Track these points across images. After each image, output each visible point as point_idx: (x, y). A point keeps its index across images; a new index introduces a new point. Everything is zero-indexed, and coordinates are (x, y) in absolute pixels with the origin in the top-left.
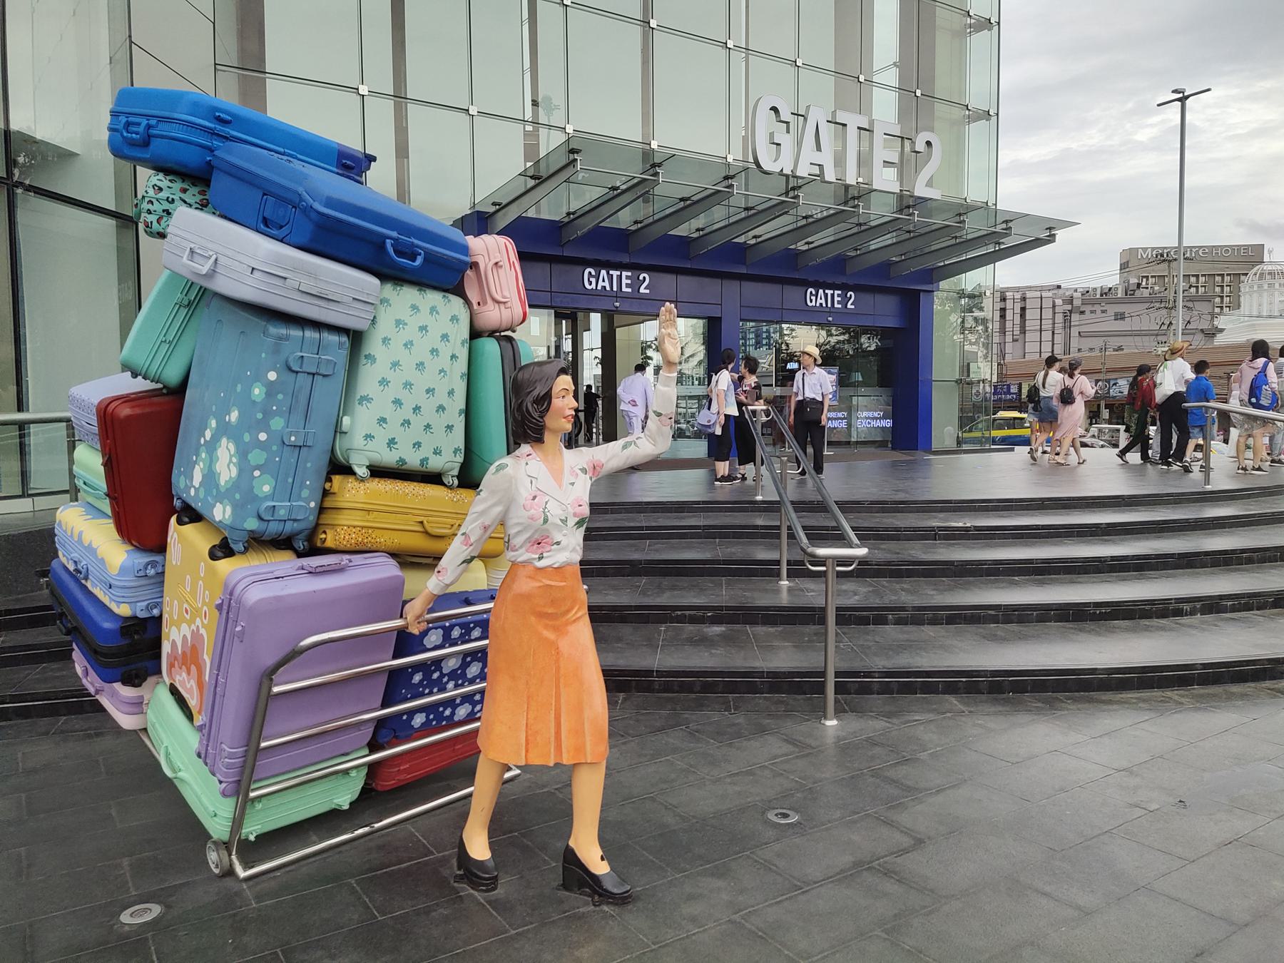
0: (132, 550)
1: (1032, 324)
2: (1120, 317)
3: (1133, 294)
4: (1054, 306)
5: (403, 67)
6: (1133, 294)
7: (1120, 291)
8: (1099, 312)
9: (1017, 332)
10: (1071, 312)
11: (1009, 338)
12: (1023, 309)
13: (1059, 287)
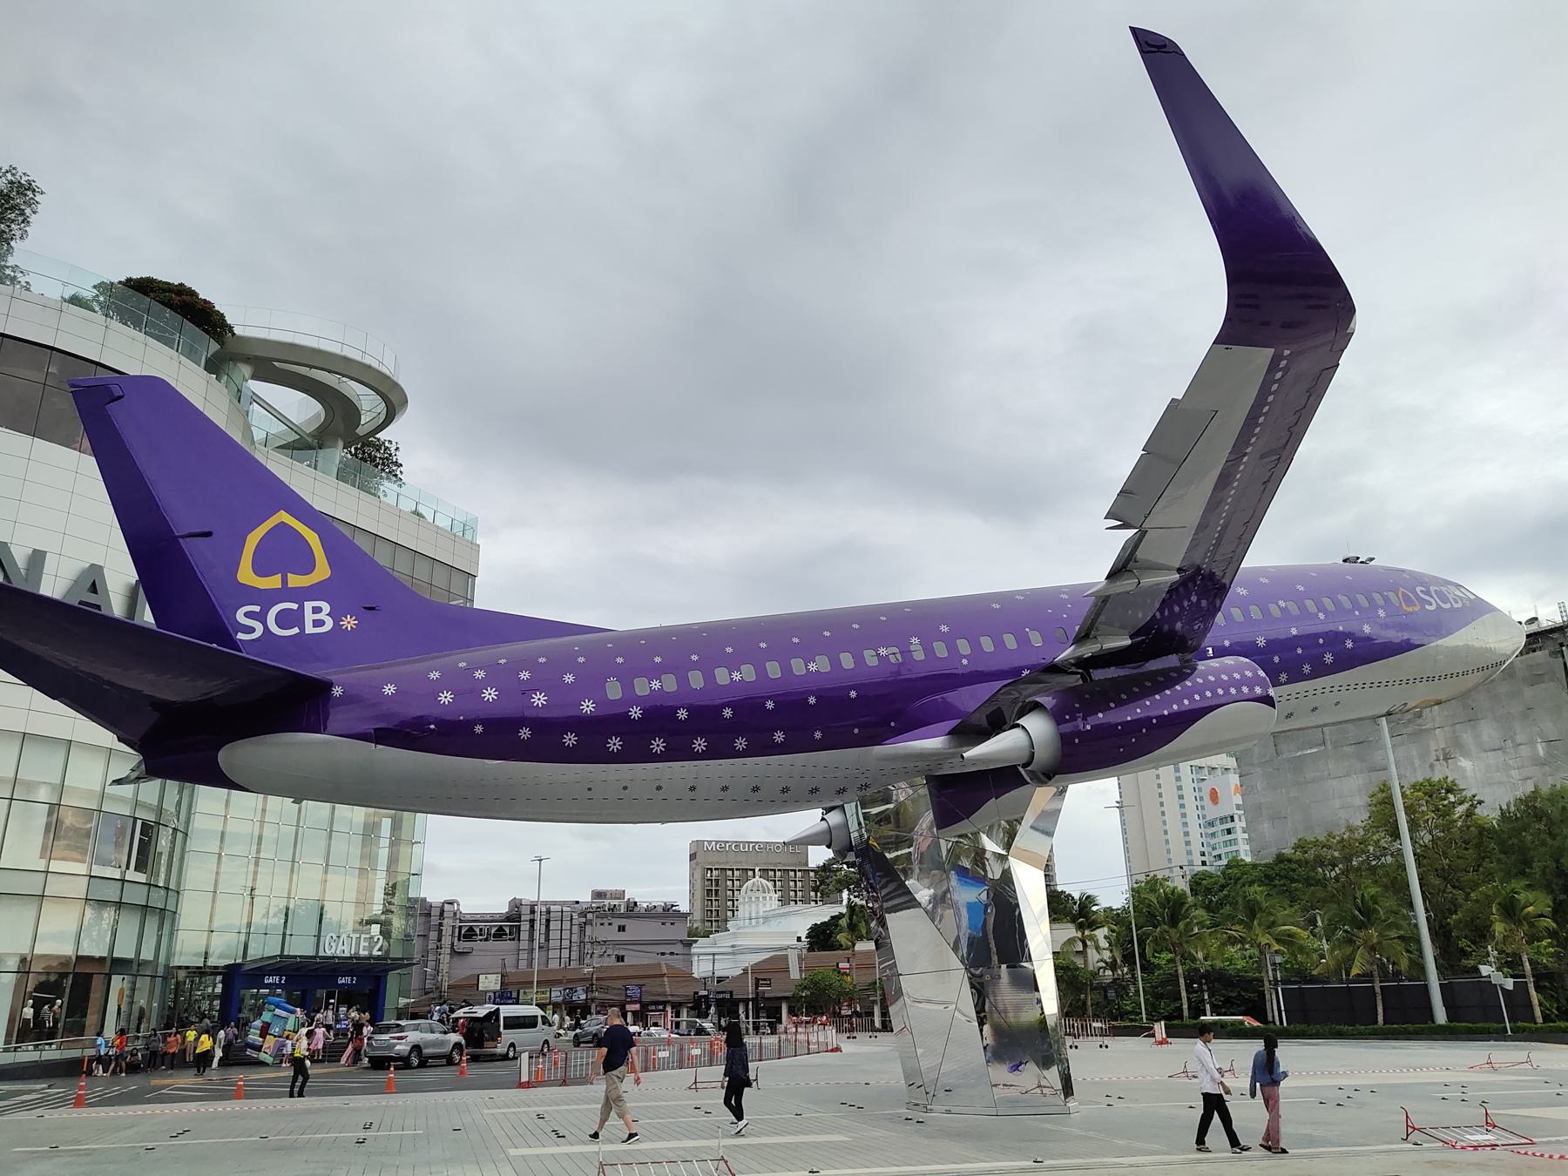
1: (554, 935)
2: (622, 929)
3: (633, 911)
4: (571, 919)
6: (633, 911)
8: (606, 924)
9: (542, 941)
10: (585, 923)
12: (548, 921)
13: (577, 902)
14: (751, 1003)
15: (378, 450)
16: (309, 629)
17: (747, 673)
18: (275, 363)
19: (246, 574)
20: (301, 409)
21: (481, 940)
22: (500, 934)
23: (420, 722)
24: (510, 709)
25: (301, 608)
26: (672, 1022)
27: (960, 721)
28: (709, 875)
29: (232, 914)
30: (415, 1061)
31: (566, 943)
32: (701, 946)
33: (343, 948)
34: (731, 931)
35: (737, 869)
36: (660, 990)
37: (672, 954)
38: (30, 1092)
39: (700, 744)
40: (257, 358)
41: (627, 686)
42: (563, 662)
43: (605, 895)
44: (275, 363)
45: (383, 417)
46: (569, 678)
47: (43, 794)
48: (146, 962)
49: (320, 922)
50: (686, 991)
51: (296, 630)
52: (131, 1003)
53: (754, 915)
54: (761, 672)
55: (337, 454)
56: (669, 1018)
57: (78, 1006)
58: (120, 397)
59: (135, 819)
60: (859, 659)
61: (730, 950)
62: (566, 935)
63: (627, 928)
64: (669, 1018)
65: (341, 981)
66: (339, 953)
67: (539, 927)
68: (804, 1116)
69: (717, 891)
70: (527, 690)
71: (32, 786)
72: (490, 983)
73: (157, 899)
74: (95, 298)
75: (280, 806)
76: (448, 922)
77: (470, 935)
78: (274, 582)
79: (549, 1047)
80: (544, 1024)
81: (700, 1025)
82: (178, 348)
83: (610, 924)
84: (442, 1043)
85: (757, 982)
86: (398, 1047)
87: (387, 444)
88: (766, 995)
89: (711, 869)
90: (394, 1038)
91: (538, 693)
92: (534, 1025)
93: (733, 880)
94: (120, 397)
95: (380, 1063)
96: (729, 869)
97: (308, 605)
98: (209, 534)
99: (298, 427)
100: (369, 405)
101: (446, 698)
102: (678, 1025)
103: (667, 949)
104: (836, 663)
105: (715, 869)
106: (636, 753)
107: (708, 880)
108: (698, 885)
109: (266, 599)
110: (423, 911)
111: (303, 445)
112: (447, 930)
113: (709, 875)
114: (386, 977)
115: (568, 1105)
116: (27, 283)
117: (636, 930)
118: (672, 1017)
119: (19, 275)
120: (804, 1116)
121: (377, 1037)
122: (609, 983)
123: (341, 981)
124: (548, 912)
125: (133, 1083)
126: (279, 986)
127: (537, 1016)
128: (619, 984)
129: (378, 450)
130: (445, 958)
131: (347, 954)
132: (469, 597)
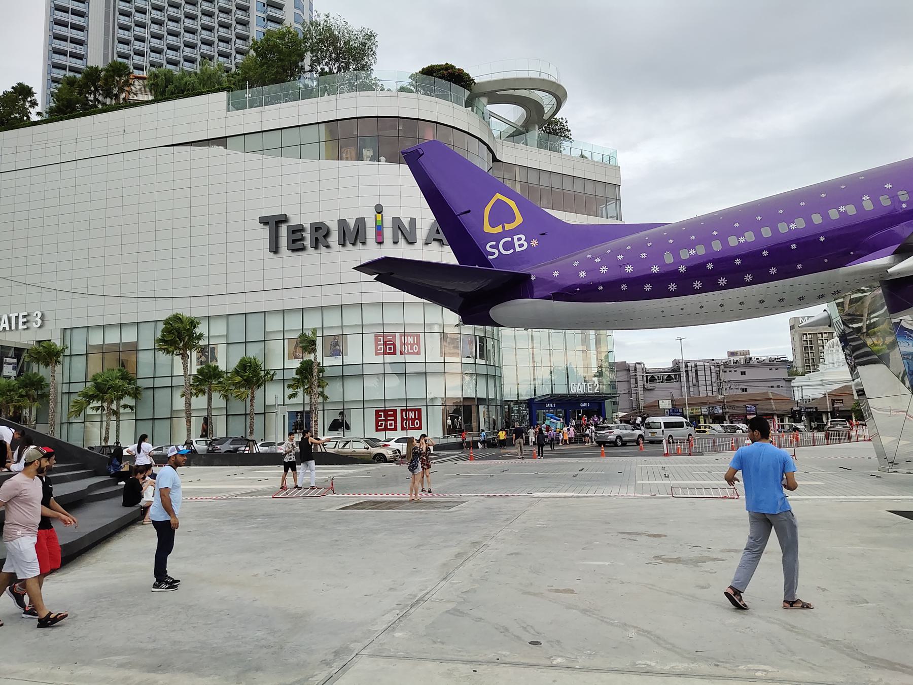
0: (736, 608)
2: (743, 373)
3: (749, 363)
4: (711, 369)
5: (788, 193)
6: (749, 363)
7: (742, 361)
8: (733, 371)
9: (695, 381)
11: (691, 384)
12: (696, 371)
13: (713, 360)
14: (829, 414)
15: (557, 125)
16: (518, 249)
17: (749, 237)
18: (497, 93)
19: (487, 228)
20: (513, 113)
21: (659, 383)
22: (669, 379)
23: (572, 288)
24: (616, 275)
25: (513, 239)
26: (779, 425)
27: (899, 245)
28: (805, 338)
29: (525, 375)
30: (620, 443)
31: (709, 382)
32: (798, 381)
33: (580, 390)
34: (821, 371)
35: (824, 333)
36: (768, 407)
37: (778, 386)
38: (454, 455)
39: (722, 281)
40: (489, 92)
41: (676, 255)
42: (640, 246)
43: (737, 354)
44: (497, 93)
45: (555, 106)
46: (643, 256)
47: (437, 329)
48: (492, 399)
49: (568, 378)
50: (786, 407)
51: (512, 251)
52: (489, 417)
53: (835, 361)
54: (758, 234)
55: (535, 133)
56: (777, 423)
57: (468, 419)
58: (423, 154)
59: (476, 336)
60: (825, 216)
61: (820, 383)
62: (708, 378)
63: (746, 373)
64: (777, 423)
65: (582, 405)
66: (578, 392)
67: (692, 374)
68: (809, 473)
69: (811, 347)
70: (622, 265)
71: (431, 325)
72: (666, 404)
73: (491, 371)
74: (411, 84)
75: (520, 332)
76: (639, 374)
77: (652, 380)
78: (499, 229)
79: (672, 438)
80: (687, 426)
81: (795, 427)
82: (451, 99)
83: (735, 371)
84: (632, 435)
85: (833, 402)
86: (610, 437)
87: (560, 120)
88: (840, 409)
89: (806, 334)
90: (607, 432)
91: (628, 266)
92: (682, 426)
93: (822, 340)
94: (423, 154)
95: (600, 443)
96: (819, 333)
97: (515, 238)
98: (469, 211)
99: (514, 124)
100: (546, 100)
101: (582, 274)
102: (783, 427)
103: (775, 384)
104: (809, 221)
105: (809, 334)
106: (685, 290)
107: (804, 341)
108: (798, 344)
109: (497, 238)
110: (624, 368)
111: (518, 133)
112: (640, 378)
113: (805, 338)
114: (604, 403)
115: (698, 464)
116: (382, 85)
117: (751, 374)
118: (778, 422)
119: (378, 82)
120: (809, 473)
121: (599, 432)
122: (736, 404)
123: (582, 405)
124: (696, 366)
125: (494, 451)
126: (552, 408)
127: (683, 422)
128: (741, 404)
129: (557, 125)
130: (641, 393)
131: (582, 392)
132: (608, 204)
